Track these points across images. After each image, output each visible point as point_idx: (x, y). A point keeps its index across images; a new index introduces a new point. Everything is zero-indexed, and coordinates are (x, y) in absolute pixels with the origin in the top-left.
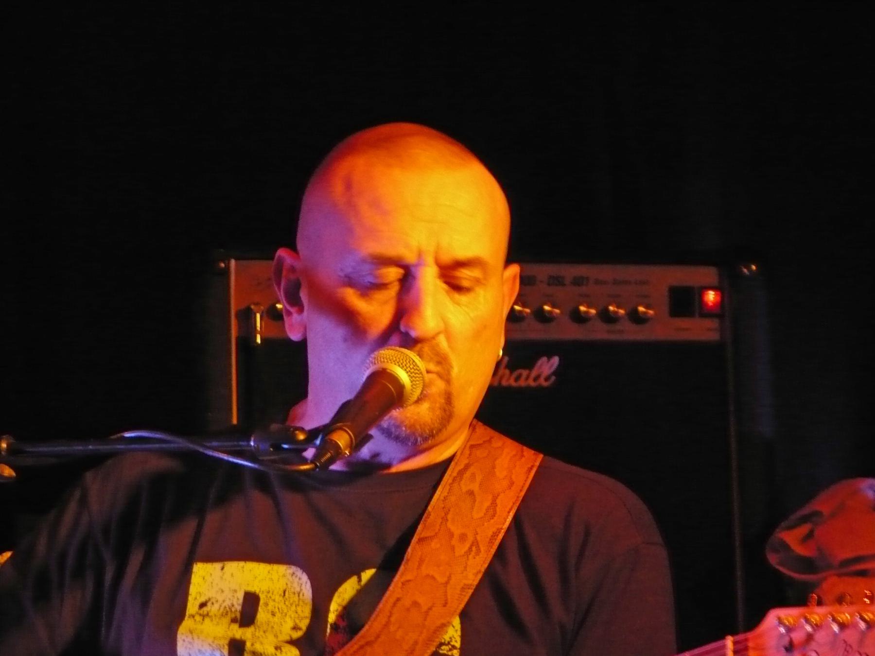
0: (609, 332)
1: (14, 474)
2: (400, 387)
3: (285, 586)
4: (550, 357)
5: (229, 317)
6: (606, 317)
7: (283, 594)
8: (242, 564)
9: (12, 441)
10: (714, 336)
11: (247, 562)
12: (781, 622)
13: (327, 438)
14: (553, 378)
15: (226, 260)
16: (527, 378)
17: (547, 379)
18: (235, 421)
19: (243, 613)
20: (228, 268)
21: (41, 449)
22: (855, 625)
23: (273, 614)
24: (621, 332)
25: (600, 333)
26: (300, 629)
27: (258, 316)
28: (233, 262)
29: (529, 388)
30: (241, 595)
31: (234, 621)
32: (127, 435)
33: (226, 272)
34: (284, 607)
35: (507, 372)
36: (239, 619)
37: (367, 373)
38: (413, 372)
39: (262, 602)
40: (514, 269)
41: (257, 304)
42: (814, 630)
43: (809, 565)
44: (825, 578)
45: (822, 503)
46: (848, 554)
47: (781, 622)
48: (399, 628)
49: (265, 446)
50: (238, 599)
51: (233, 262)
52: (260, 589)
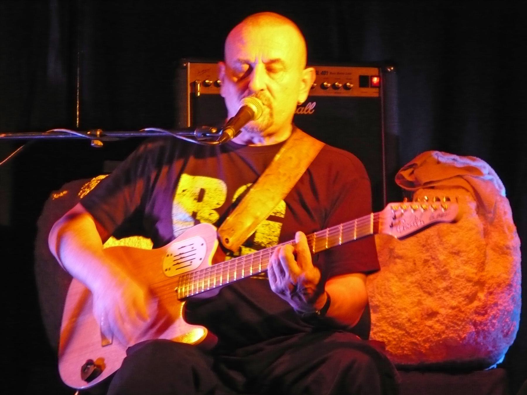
0: (335, 93)
1: (102, 144)
2: (253, 113)
4: (312, 103)
5: (187, 85)
6: (334, 87)
9: (101, 131)
10: (376, 95)
12: (392, 208)
13: (224, 132)
14: (313, 111)
15: (187, 63)
17: (311, 111)
18: (189, 126)
20: (187, 66)
21: (112, 135)
22: (420, 210)
24: (340, 93)
25: (332, 93)
27: (199, 85)
28: (189, 64)
29: (303, 114)
32: (146, 129)
33: (186, 67)
37: (240, 107)
38: (258, 107)
40: (311, 69)
41: (198, 80)
42: (404, 212)
43: (411, 184)
44: (418, 190)
45: (418, 161)
46: (428, 180)
47: (392, 208)
49: (200, 134)
51: (189, 64)
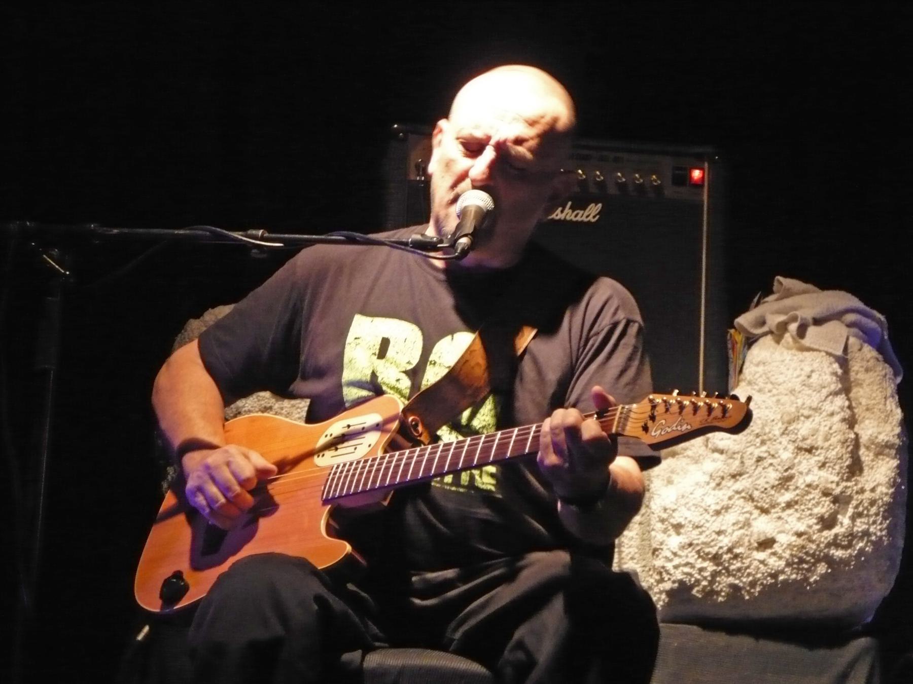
17: (594, 217)
31: (374, 354)
35: (570, 211)
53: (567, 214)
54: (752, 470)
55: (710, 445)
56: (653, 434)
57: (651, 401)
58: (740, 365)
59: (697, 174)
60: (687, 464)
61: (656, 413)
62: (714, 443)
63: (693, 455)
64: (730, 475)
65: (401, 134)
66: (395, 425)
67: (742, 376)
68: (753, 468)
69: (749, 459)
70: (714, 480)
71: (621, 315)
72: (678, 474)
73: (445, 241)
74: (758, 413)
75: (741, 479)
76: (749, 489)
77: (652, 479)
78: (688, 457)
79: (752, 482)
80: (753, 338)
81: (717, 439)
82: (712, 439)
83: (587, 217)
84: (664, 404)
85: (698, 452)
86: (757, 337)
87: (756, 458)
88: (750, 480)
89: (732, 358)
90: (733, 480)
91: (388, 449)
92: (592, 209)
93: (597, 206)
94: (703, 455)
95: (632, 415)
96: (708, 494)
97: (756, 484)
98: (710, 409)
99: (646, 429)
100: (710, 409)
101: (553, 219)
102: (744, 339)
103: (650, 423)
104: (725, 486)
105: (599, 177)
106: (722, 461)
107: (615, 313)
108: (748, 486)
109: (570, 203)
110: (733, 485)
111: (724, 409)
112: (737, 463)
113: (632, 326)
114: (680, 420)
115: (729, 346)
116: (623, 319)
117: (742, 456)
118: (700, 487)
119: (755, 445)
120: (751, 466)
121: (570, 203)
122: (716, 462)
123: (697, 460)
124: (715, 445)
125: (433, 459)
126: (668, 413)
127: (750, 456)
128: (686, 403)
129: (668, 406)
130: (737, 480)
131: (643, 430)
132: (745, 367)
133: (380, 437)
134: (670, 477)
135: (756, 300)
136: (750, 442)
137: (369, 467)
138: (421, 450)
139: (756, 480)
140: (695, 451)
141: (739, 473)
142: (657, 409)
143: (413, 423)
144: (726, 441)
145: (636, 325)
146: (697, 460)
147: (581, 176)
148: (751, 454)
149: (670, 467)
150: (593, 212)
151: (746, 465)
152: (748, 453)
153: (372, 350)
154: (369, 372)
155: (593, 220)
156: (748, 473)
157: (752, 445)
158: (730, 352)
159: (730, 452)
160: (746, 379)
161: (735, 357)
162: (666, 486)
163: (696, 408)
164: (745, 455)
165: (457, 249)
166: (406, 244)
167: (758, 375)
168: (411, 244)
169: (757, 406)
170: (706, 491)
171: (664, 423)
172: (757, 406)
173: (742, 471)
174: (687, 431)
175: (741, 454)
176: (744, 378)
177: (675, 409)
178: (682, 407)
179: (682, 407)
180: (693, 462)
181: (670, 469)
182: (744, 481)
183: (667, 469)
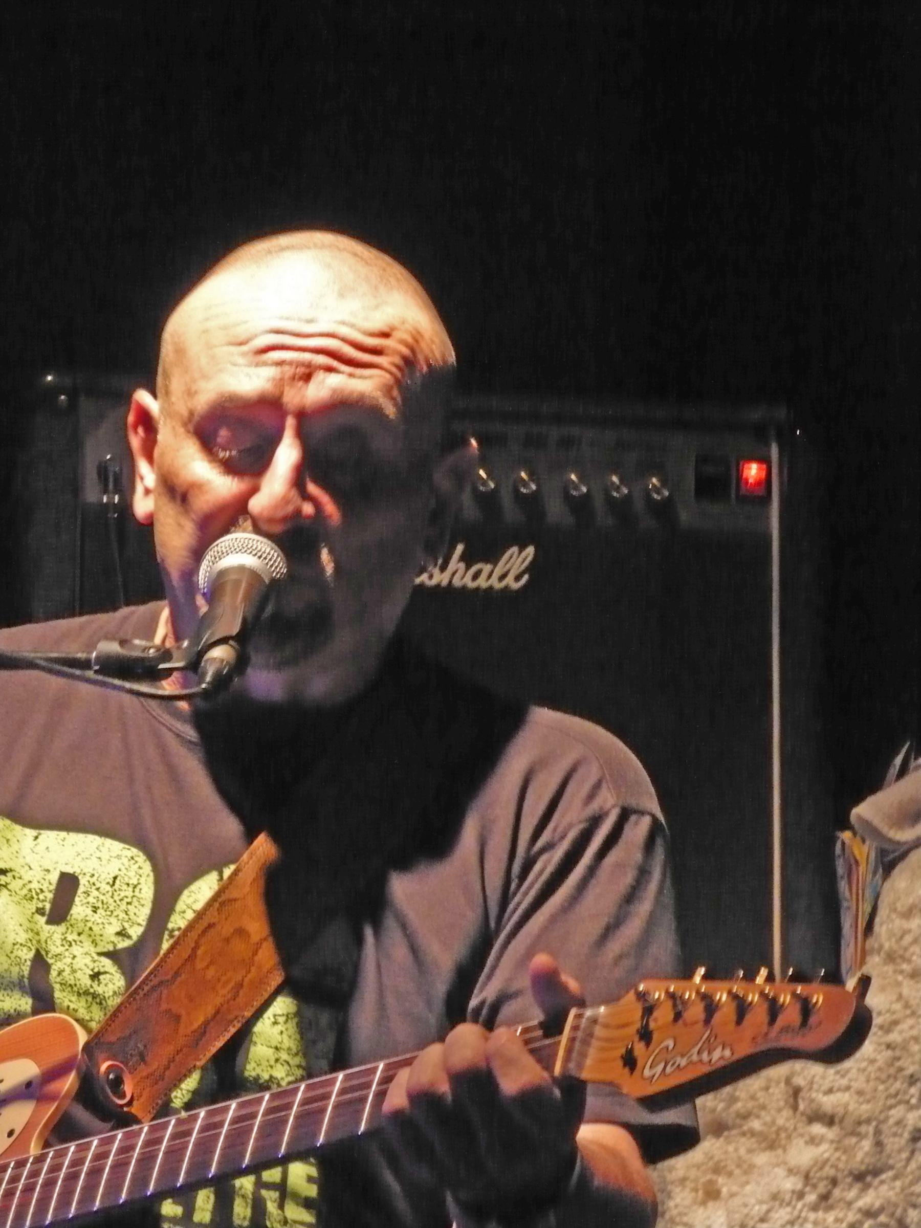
3: (117, 872)
7: (111, 883)
8: (63, 834)
11: (71, 834)
16: (490, 576)
17: (518, 578)
19: (55, 903)
23: (95, 910)
26: (129, 937)
30: (54, 877)
31: (40, 911)
34: (111, 900)
35: (462, 565)
36: (47, 912)
39: (81, 889)
48: (211, 963)
50: (50, 883)
52: (82, 870)
53: (454, 574)
54: (901, 1160)
55: (802, 1107)
56: (647, 1073)
57: (642, 997)
58: (867, 917)
59: (753, 471)
60: (750, 1151)
61: (652, 1025)
62: (812, 1101)
63: (764, 1129)
64: (851, 1173)
65: (63, 397)
66: (69, 1082)
67: (871, 942)
68: (904, 1155)
69: (895, 1135)
70: (815, 1186)
71: (608, 800)
72: (730, 1174)
73: (175, 654)
74: (912, 1027)
75: (876, 1182)
76: (896, 1205)
77: (669, 1187)
78: (752, 1133)
79: (903, 1190)
80: (894, 851)
81: (817, 1091)
82: (805, 1090)
83: (502, 577)
84: (670, 1003)
85: (773, 1122)
86: (905, 848)
87: (910, 1133)
88: (898, 1184)
89: (847, 900)
90: (858, 1186)
91: (52, 1140)
92: (512, 560)
93: (524, 554)
94: (786, 1130)
95: (598, 1031)
96: (800, 1221)
97: (912, 1194)
98: (774, 1009)
99: (630, 1061)
100: (774, 1009)
101: (422, 586)
102: (873, 855)
103: (639, 1049)
104: (840, 1200)
105: (525, 485)
106: (832, 1142)
107: (591, 797)
108: (894, 1199)
109: (460, 548)
110: (858, 1197)
111: (806, 1008)
112: (867, 1145)
113: (636, 823)
114: (708, 1038)
115: (841, 870)
116: (614, 806)
117: (877, 1127)
118: (781, 1205)
119: (908, 1102)
120: (900, 1151)
121: (460, 548)
122: (818, 1145)
123: (774, 1141)
124: (814, 1106)
125: (152, 1157)
126: (680, 1022)
127: (895, 1129)
128: (722, 997)
129: (680, 1007)
130: (867, 1187)
131: (625, 1065)
132: (877, 920)
133: (35, 1107)
134: (711, 1182)
135: (898, 760)
136: (897, 1094)
137: (8, 1183)
138: (127, 1136)
139: (912, 1183)
140: (768, 1119)
141: (871, 1167)
142: (656, 1014)
143: (111, 1076)
144: (839, 1095)
145: (646, 821)
146: (774, 1141)
147: (484, 483)
148: (899, 1123)
149: (712, 1158)
150: (515, 567)
151: (888, 1148)
152: (891, 1121)
153: (35, 901)
154: (27, 955)
155: (515, 586)
156: (891, 1168)
157: (900, 1103)
158: (843, 886)
159: (848, 1122)
160: (881, 947)
161: (854, 896)
162: (704, 1203)
163: (742, 1008)
164: (884, 1127)
165: (204, 674)
166: (85, 665)
167: (908, 939)
168: (96, 664)
169: (908, 1012)
170: (796, 1213)
171: (671, 1047)
172: (908, 1012)
173: (879, 1165)
174: (722, 1063)
175: (874, 1124)
176: (876, 946)
177: (696, 1011)
178: (711, 1008)
179: (711, 1008)
180: (764, 1145)
181: (711, 1164)
182: (884, 1187)
183: (703, 1164)
